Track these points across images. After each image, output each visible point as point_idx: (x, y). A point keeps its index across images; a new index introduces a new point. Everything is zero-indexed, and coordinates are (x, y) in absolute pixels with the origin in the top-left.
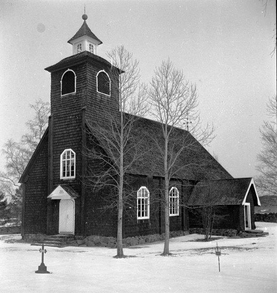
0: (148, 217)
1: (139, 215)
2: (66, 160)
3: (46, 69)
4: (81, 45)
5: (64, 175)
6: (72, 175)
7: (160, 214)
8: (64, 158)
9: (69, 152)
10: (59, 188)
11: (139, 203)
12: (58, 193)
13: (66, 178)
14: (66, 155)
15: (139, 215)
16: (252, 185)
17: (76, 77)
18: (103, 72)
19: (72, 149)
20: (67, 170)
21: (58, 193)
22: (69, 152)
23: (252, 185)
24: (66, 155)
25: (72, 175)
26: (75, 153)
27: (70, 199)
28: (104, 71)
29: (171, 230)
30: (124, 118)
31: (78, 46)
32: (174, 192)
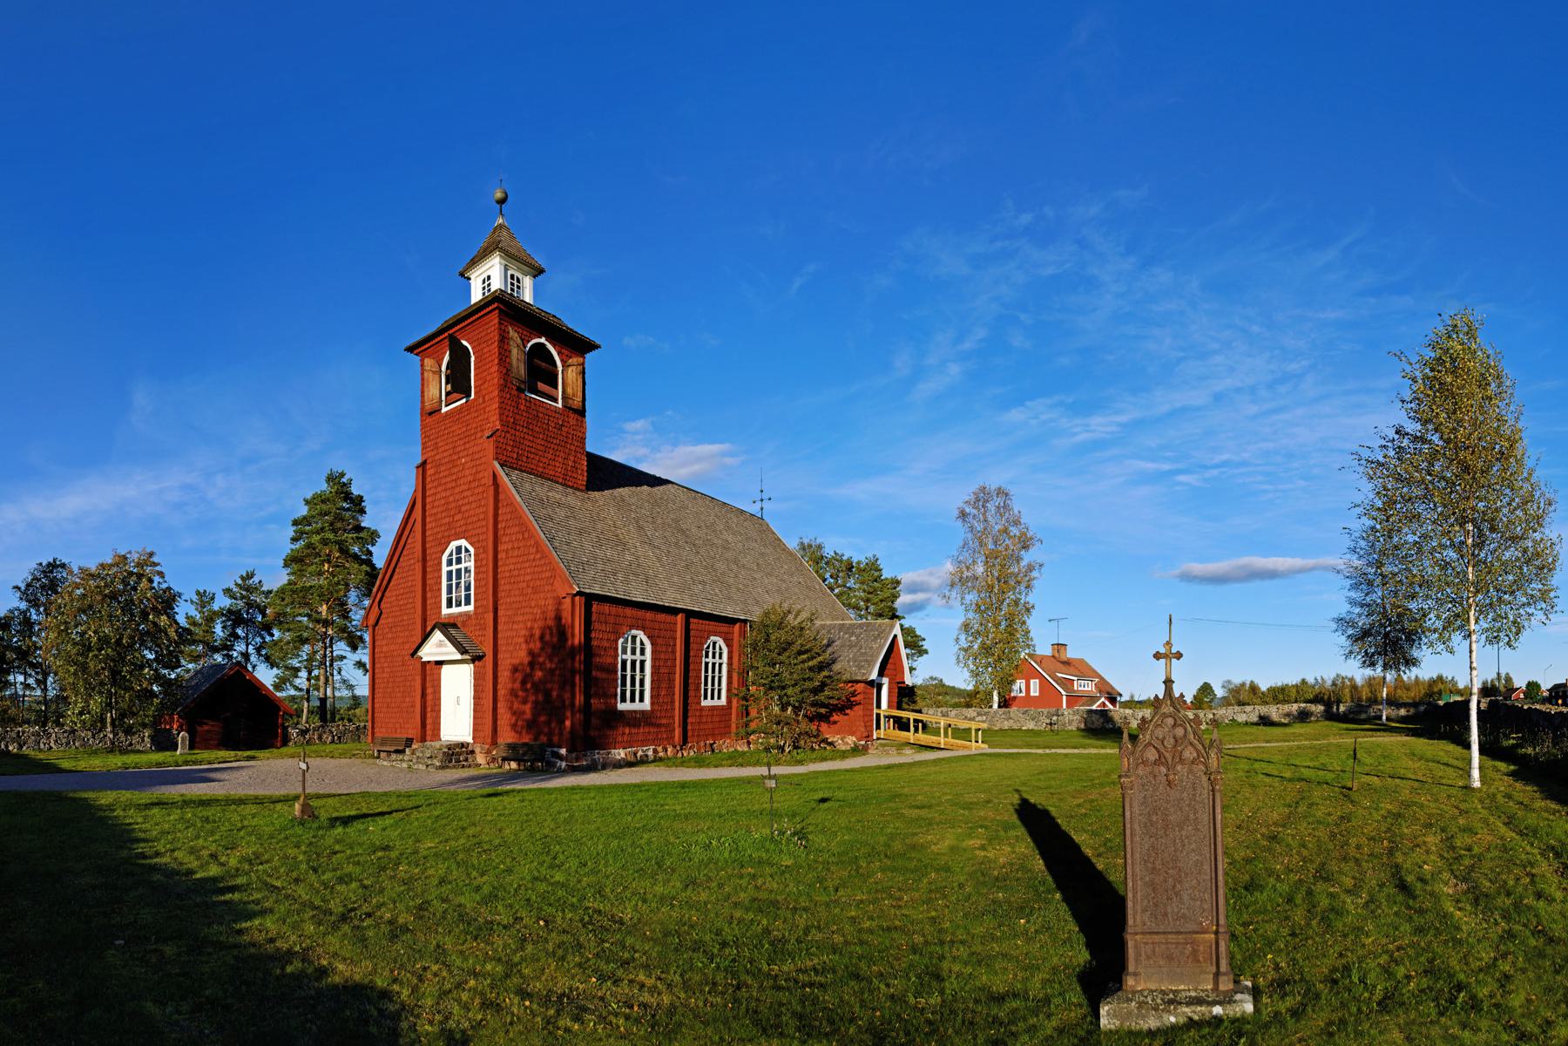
0: (647, 705)
1: (623, 700)
4: (489, 278)
5: (449, 605)
8: (450, 563)
12: (436, 647)
13: (455, 610)
14: (454, 557)
15: (623, 700)
16: (895, 636)
17: (473, 359)
18: (543, 344)
19: (466, 539)
21: (436, 647)
23: (895, 636)
24: (454, 557)
25: (468, 603)
26: (472, 550)
28: (543, 340)
29: (940, 728)
30: (739, 660)
31: (484, 282)
32: (714, 648)
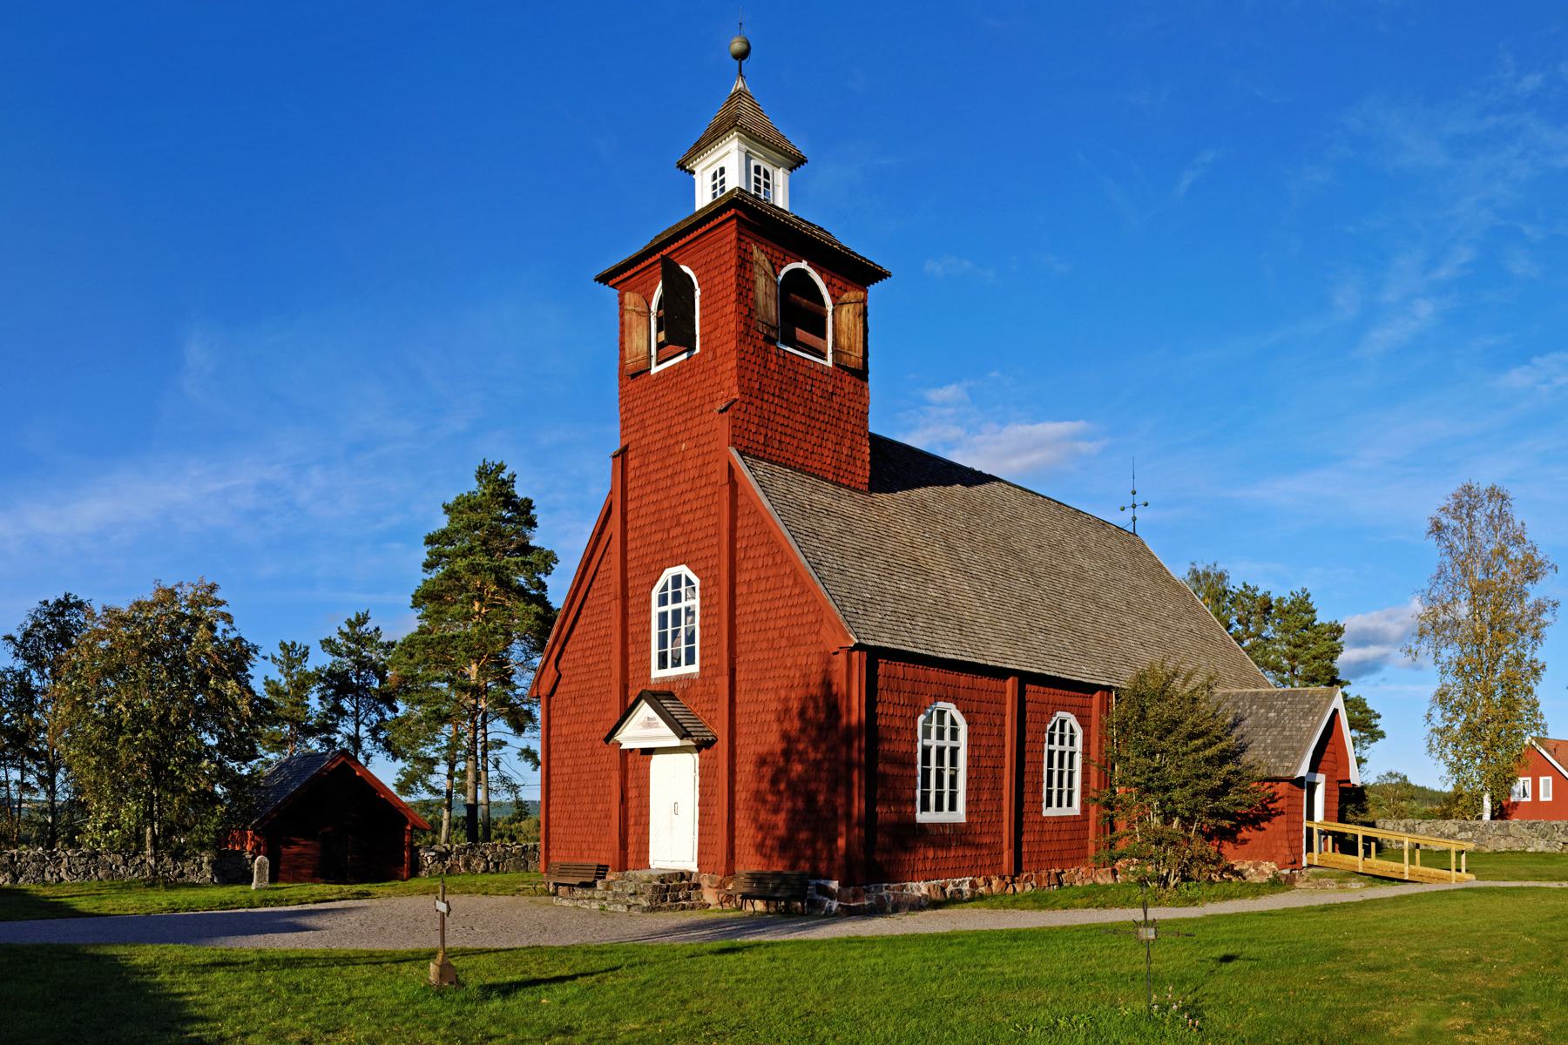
1: (925, 807)
2: (670, 607)
3: (596, 280)
4: (722, 171)
5: (663, 664)
6: (690, 661)
7: (602, 953)
8: (663, 601)
9: (680, 576)
10: (645, 711)
11: (926, 760)
13: (670, 672)
14: (670, 592)
16: (1336, 711)
17: (698, 293)
18: (803, 272)
19: (688, 565)
20: (929, 770)
22: (680, 576)
24: (670, 592)
25: (690, 661)
26: (696, 581)
27: (619, 737)
28: (803, 265)
31: (715, 177)
32: (1062, 729)
